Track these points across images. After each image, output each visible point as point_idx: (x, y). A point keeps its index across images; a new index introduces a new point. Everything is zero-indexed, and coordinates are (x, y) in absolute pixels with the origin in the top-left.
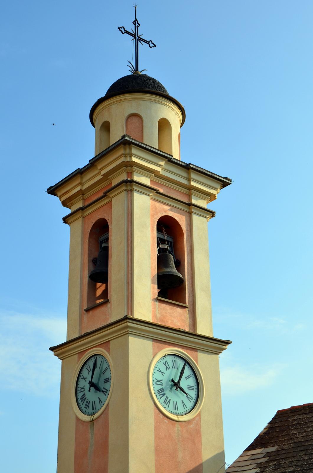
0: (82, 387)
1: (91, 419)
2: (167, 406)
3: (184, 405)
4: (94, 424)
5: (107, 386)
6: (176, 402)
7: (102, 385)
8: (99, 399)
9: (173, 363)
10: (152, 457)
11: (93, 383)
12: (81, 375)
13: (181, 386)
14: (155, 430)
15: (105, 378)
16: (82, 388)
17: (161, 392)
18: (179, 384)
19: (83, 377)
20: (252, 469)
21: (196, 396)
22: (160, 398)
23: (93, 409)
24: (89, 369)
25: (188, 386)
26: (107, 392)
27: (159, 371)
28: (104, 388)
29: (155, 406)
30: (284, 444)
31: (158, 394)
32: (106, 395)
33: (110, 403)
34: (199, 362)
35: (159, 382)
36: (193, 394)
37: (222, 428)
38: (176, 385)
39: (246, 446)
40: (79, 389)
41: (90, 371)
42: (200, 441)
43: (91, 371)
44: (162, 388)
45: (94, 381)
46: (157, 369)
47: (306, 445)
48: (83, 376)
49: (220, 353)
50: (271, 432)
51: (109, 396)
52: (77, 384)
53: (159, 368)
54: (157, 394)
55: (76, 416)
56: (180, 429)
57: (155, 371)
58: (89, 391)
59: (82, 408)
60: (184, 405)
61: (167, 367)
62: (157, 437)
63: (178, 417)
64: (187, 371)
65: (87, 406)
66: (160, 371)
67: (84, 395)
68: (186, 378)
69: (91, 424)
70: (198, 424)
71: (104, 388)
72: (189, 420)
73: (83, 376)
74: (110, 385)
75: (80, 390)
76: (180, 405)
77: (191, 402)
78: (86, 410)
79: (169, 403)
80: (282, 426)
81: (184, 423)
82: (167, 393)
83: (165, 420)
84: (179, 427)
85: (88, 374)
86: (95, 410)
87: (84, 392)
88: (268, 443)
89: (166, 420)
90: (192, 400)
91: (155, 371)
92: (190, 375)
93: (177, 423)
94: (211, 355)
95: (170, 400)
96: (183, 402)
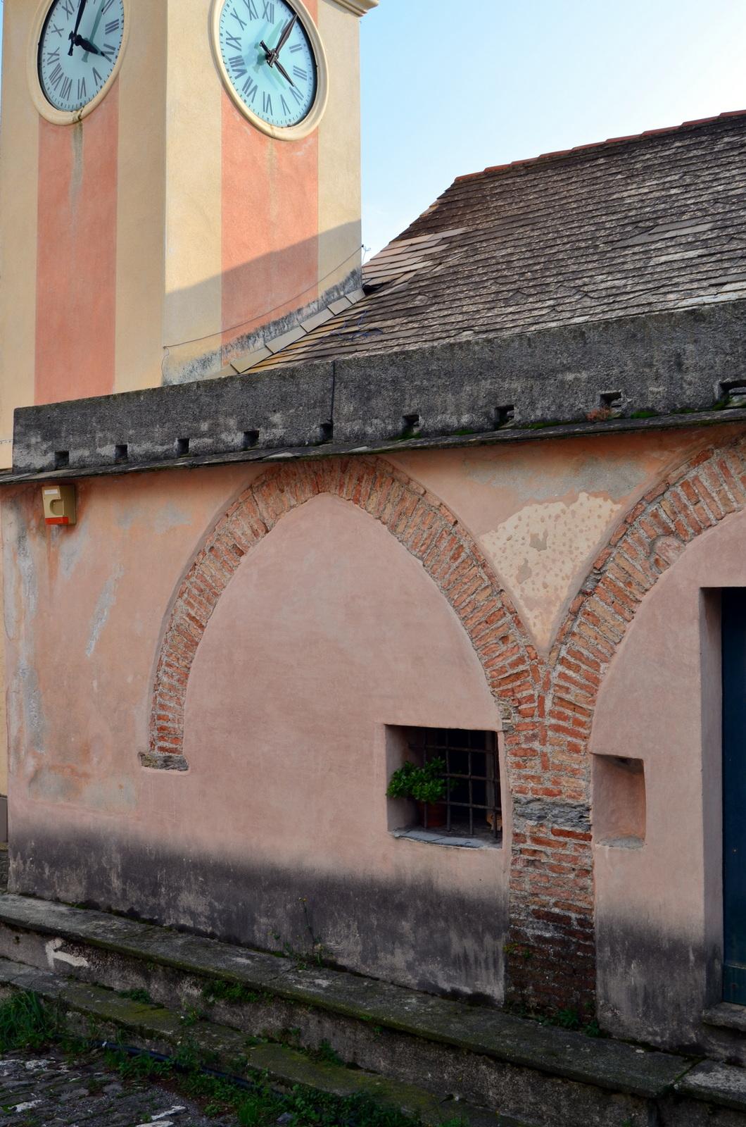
0: (58, 28)
1: (77, 118)
2: (249, 99)
3: (285, 107)
4: (83, 127)
5: (112, 39)
6: (269, 96)
7: (99, 42)
8: (95, 71)
9: (266, 8)
10: (217, 200)
11: (80, 36)
12: (50, 24)
13: (279, 60)
14: (222, 142)
15: (107, 23)
16: (52, 54)
17: (237, 62)
18: (278, 56)
19: (55, 29)
20: (415, 263)
21: (310, 94)
22: (236, 78)
23: (79, 97)
24: (70, 9)
25: (294, 67)
26: (112, 53)
27: (234, 16)
28: (105, 45)
29: (223, 89)
30: (478, 222)
31: (232, 66)
32: (110, 60)
33: (120, 76)
34: (319, 22)
35: (233, 41)
36: (304, 87)
37: (359, 174)
38: (269, 56)
39: (405, 226)
40: (45, 57)
41: (72, 11)
42: (316, 190)
43: (74, 10)
44: (240, 57)
45: (83, 32)
46: (230, 10)
47: (530, 218)
48: (54, 26)
49: (364, 13)
50: (447, 209)
51: (118, 61)
52: (41, 45)
53: (234, 9)
54: (229, 66)
55: (40, 115)
56: (275, 153)
57: (225, 13)
58: (70, 53)
59: (54, 99)
60: (285, 107)
61: (251, 12)
62: (228, 159)
63: (272, 129)
64: (295, 36)
65: (65, 93)
66: (237, 17)
67: (59, 68)
68: (290, 48)
69: (76, 129)
70: (313, 151)
71: (105, 45)
72: (295, 141)
73: (54, 26)
74: (122, 36)
75: (49, 59)
76: (276, 103)
77: (299, 104)
78: (64, 101)
79: (253, 93)
80: (470, 198)
81: (283, 144)
82: (250, 68)
83: (246, 128)
84: (274, 149)
85: (61, 36)
86: (84, 99)
87: (57, 62)
88: (443, 225)
89: (247, 128)
90: (302, 99)
91: (225, 13)
92: (300, 45)
93: (270, 139)
94: (345, 13)
95: (256, 88)
96: (283, 100)
